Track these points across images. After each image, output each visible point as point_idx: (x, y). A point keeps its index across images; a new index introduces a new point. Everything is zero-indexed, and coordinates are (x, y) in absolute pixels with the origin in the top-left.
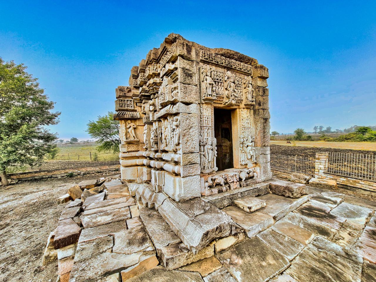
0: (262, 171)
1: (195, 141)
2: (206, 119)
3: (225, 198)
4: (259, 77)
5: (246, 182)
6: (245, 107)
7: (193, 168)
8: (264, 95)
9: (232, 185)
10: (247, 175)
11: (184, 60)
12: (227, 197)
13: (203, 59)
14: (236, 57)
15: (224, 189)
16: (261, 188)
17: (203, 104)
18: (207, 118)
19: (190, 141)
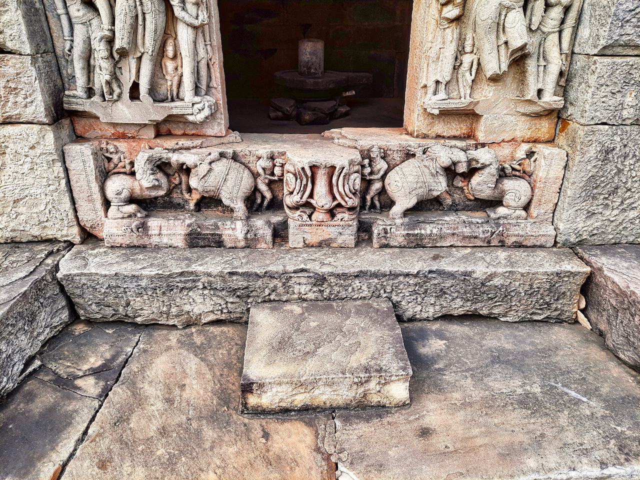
0: (578, 176)
3: (189, 285)
9: (295, 219)
10: (440, 186)
12: (204, 279)
15: (234, 231)
16: (497, 281)
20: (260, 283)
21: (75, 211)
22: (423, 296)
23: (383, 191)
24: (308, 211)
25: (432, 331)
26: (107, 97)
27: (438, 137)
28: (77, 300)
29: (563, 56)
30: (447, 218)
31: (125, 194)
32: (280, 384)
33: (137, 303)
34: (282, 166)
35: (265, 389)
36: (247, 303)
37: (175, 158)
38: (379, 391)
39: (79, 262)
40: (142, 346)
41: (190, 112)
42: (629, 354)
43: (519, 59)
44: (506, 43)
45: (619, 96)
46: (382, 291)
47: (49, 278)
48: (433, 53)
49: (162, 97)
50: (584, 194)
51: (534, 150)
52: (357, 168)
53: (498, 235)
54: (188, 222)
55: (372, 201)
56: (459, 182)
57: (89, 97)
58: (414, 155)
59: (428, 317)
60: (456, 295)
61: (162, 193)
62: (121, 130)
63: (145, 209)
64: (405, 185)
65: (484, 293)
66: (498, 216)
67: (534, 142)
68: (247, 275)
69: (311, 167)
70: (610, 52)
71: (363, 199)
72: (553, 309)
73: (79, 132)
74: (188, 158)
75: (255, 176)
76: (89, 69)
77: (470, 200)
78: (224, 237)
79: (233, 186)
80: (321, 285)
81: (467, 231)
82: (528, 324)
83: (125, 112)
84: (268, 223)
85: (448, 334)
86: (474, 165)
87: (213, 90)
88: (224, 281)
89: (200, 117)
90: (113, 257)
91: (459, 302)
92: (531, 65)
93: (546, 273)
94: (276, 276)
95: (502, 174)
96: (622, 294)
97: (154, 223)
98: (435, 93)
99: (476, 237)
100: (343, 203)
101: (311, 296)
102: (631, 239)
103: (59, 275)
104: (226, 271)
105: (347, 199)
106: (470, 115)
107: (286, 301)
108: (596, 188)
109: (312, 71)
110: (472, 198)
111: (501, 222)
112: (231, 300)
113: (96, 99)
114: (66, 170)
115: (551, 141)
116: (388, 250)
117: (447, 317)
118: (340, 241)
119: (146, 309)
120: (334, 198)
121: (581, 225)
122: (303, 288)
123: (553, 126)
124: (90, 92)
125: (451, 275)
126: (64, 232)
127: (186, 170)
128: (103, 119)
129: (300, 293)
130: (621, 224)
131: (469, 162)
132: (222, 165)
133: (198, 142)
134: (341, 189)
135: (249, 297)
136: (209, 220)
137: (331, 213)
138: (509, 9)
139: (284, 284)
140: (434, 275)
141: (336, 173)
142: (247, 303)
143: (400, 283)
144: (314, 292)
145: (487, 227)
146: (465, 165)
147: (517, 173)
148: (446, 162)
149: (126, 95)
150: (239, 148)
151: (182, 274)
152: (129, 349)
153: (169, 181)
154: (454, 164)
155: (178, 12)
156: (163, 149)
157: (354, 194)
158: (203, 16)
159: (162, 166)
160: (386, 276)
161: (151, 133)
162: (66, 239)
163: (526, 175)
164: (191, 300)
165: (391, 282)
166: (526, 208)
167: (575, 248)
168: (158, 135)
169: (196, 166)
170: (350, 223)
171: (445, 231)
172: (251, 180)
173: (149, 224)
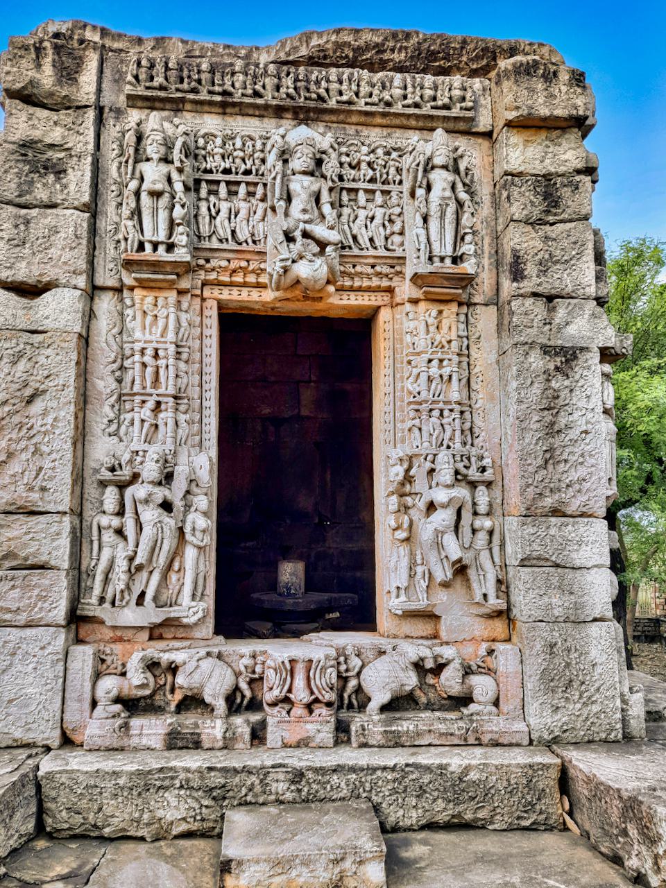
1: (54, 456)
2: (148, 359)
3: (167, 783)
4: (509, 124)
5: (388, 723)
6: (417, 293)
7: (22, 588)
8: (551, 219)
9: (274, 717)
11: (32, 109)
12: (182, 776)
13: (140, 91)
14: (398, 57)
15: (213, 729)
16: (473, 776)
17: (132, 289)
18: (150, 352)
19: (23, 456)
20: (237, 779)
21: (63, 712)
22: (403, 795)
23: (359, 690)
24: (287, 707)
25: (416, 840)
26: (117, 603)
27: (407, 637)
28: (49, 805)
29: (498, 568)
30: (422, 715)
31: (114, 693)
32: (257, 862)
33: (110, 806)
34: (263, 663)
35: (243, 867)
36: (221, 807)
37: (165, 658)
38: (355, 873)
39: (59, 762)
40: (109, 857)
41: (185, 615)
42: (607, 844)
43: (461, 570)
44: (447, 557)
45: (546, 598)
46: (361, 790)
47: (31, 775)
48: (392, 564)
49: (162, 603)
50: (542, 687)
51: (493, 648)
52: (333, 662)
53: (473, 731)
54: (169, 721)
55: (347, 701)
56: (430, 680)
57: (100, 605)
58: (384, 652)
59: (412, 825)
60: (436, 794)
61: (147, 692)
62: (119, 633)
63: (128, 710)
64: (380, 681)
65: (463, 791)
66: (470, 712)
67: (493, 640)
68: (225, 770)
69: (290, 661)
70: (529, 564)
71: (341, 697)
72: (538, 811)
73: (81, 636)
74: (178, 657)
75: (237, 674)
76: (106, 580)
77: (445, 699)
78: (203, 736)
79: (215, 690)
80: (299, 782)
81: (442, 727)
82: (518, 833)
83: (130, 616)
84: (247, 721)
85: (432, 842)
86: (441, 661)
87: (206, 598)
88: (202, 778)
89: (193, 619)
90: (91, 757)
91: (440, 804)
92: (472, 573)
93: (518, 765)
94: (254, 771)
95: (467, 672)
96: (589, 780)
97: (136, 722)
98: (398, 596)
99: (452, 734)
100: (321, 697)
101: (289, 796)
102: (603, 736)
103: (40, 773)
104: (205, 766)
105: (324, 692)
106: (430, 616)
107: (263, 804)
108: (552, 681)
109: (293, 591)
110: (445, 696)
111: (474, 718)
112: (205, 802)
113: (107, 605)
114: (66, 669)
115: (509, 640)
116: (366, 750)
117: (431, 826)
118: (318, 740)
119: (118, 815)
120: (312, 693)
121: (549, 721)
122: (280, 786)
123: (506, 626)
124: (102, 600)
125: (428, 769)
126: (46, 735)
127: (173, 669)
128: (109, 623)
129: (277, 793)
130: (587, 718)
131: (435, 658)
132: (208, 667)
133: (187, 643)
134: (318, 682)
135: (224, 798)
136: (189, 720)
137: (309, 707)
138: (443, 533)
139: (261, 781)
140: (411, 769)
141: (314, 666)
142: (221, 807)
143: (379, 779)
144: (292, 791)
145: (461, 724)
146: (431, 660)
147: (483, 670)
148: (415, 658)
149: (134, 601)
150: (223, 649)
151: (161, 770)
152: (96, 861)
153: (156, 682)
154: (422, 659)
155: (188, 537)
156: (155, 651)
157: (331, 689)
158: (207, 540)
159: (152, 666)
160: (363, 770)
161: (146, 635)
162: (45, 742)
163: (490, 671)
164: (165, 804)
165: (369, 778)
166: (496, 703)
167: (551, 744)
168: (151, 638)
169: (185, 663)
170: (328, 718)
171: (422, 727)
172: (233, 678)
173: (132, 724)
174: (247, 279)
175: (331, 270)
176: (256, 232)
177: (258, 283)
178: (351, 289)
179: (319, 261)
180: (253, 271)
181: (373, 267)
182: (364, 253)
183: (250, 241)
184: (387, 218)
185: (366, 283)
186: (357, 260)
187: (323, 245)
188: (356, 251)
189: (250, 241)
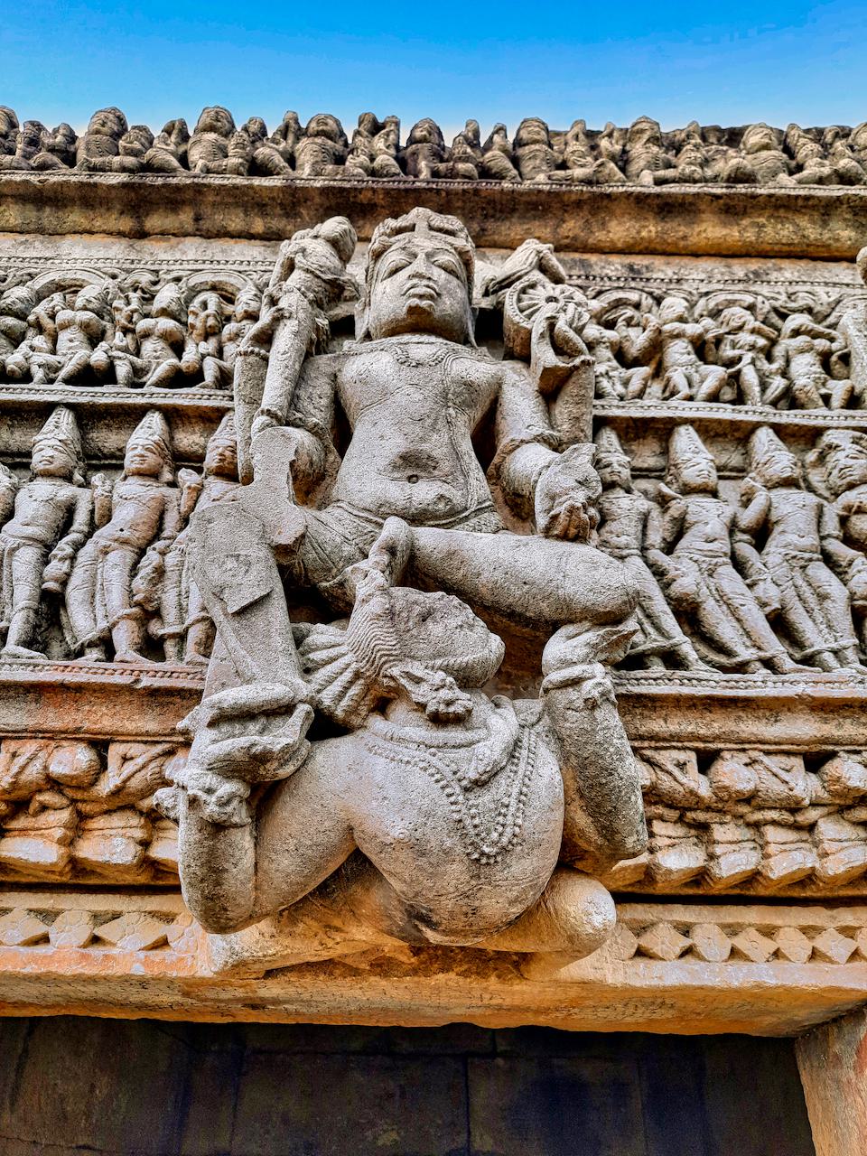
174: (89, 850)
175: (590, 786)
176: (169, 600)
177: (76, 865)
178: (699, 891)
179: (500, 723)
180: (122, 801)
181: (815, 761)
182: (760, 685)
183: (124, 639)
184: (832, 526)
185: (786, 859)
186: (718, 724)
187: (523, 631)
188: (705, 680)
189: (124, 639)
